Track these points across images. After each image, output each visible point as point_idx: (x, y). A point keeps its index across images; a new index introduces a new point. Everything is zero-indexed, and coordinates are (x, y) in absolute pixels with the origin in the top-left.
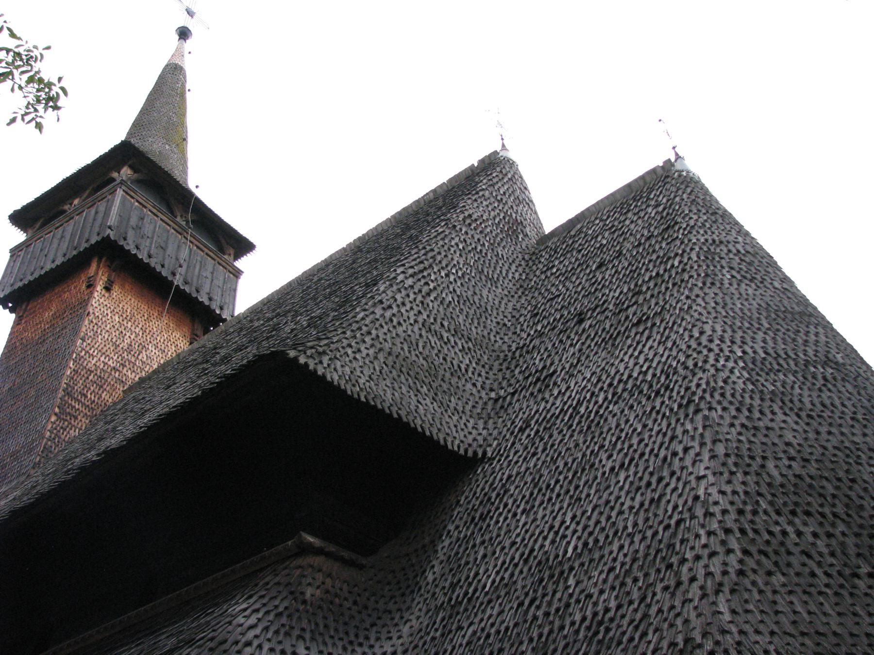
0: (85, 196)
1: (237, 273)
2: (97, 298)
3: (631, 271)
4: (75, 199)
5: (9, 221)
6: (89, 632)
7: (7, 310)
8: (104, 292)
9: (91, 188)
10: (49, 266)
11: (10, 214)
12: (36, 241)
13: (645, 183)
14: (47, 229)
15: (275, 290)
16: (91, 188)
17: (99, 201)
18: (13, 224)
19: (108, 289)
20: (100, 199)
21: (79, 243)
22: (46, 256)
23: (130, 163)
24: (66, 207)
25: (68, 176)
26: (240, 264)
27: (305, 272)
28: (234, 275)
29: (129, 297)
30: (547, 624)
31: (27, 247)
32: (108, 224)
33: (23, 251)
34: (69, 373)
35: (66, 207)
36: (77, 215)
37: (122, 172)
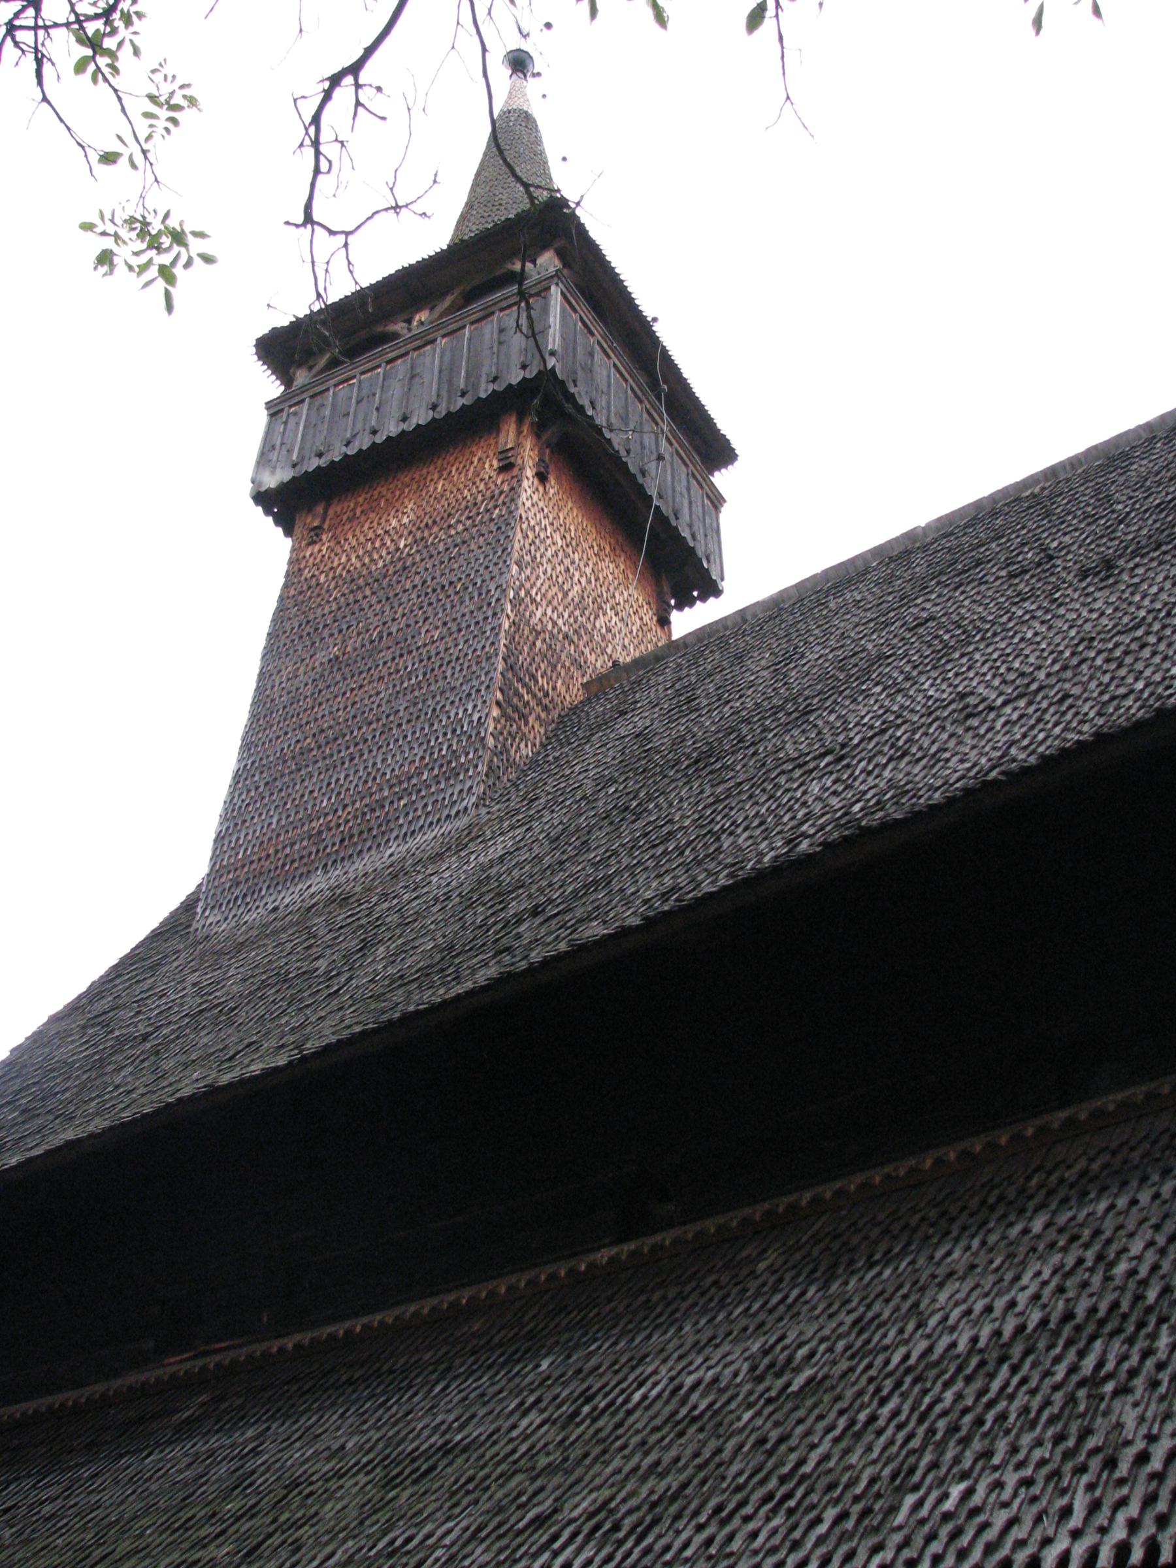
0: (440, 309)
1: (716, 501)
2: (529, 491)
3: (877, 765)
4: (419, 310)
5: (254, 350)
6: (886, 1170)
7: (270, 519)
8: (536, 482)
9: (457, 292)
10: (393, 429)
11: (260, 335)
12: (336, 386)
13: (745, 621)
14: (341, 373)
15: (1012, 482)
16: (457, 292)
17: (502, 310)
18: (260, 358)
19: (542, 477)
20: (504, 304)
21: (476, 386)
22: (377, 409)
23: (557, 245)
24: (399, 327)
25: (413, 262)
26: (721, 479)
27: (1095, 447)
28: (712, 502)
29: (570, 505)
30: (702, 1560)
31: (312, 397)
32: (550, 347)
33: (305, 406)
34: (507, 626)
35: (399, 327)
36: (444, 336)
37: (539, 261)
